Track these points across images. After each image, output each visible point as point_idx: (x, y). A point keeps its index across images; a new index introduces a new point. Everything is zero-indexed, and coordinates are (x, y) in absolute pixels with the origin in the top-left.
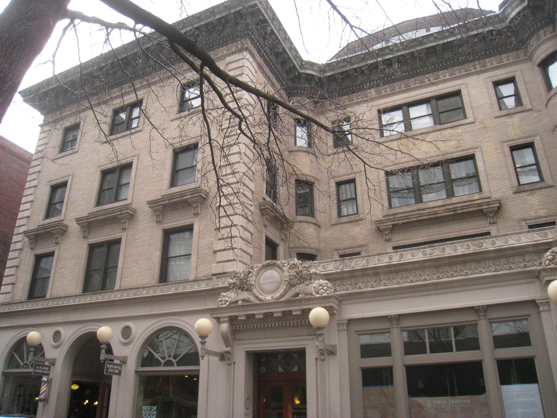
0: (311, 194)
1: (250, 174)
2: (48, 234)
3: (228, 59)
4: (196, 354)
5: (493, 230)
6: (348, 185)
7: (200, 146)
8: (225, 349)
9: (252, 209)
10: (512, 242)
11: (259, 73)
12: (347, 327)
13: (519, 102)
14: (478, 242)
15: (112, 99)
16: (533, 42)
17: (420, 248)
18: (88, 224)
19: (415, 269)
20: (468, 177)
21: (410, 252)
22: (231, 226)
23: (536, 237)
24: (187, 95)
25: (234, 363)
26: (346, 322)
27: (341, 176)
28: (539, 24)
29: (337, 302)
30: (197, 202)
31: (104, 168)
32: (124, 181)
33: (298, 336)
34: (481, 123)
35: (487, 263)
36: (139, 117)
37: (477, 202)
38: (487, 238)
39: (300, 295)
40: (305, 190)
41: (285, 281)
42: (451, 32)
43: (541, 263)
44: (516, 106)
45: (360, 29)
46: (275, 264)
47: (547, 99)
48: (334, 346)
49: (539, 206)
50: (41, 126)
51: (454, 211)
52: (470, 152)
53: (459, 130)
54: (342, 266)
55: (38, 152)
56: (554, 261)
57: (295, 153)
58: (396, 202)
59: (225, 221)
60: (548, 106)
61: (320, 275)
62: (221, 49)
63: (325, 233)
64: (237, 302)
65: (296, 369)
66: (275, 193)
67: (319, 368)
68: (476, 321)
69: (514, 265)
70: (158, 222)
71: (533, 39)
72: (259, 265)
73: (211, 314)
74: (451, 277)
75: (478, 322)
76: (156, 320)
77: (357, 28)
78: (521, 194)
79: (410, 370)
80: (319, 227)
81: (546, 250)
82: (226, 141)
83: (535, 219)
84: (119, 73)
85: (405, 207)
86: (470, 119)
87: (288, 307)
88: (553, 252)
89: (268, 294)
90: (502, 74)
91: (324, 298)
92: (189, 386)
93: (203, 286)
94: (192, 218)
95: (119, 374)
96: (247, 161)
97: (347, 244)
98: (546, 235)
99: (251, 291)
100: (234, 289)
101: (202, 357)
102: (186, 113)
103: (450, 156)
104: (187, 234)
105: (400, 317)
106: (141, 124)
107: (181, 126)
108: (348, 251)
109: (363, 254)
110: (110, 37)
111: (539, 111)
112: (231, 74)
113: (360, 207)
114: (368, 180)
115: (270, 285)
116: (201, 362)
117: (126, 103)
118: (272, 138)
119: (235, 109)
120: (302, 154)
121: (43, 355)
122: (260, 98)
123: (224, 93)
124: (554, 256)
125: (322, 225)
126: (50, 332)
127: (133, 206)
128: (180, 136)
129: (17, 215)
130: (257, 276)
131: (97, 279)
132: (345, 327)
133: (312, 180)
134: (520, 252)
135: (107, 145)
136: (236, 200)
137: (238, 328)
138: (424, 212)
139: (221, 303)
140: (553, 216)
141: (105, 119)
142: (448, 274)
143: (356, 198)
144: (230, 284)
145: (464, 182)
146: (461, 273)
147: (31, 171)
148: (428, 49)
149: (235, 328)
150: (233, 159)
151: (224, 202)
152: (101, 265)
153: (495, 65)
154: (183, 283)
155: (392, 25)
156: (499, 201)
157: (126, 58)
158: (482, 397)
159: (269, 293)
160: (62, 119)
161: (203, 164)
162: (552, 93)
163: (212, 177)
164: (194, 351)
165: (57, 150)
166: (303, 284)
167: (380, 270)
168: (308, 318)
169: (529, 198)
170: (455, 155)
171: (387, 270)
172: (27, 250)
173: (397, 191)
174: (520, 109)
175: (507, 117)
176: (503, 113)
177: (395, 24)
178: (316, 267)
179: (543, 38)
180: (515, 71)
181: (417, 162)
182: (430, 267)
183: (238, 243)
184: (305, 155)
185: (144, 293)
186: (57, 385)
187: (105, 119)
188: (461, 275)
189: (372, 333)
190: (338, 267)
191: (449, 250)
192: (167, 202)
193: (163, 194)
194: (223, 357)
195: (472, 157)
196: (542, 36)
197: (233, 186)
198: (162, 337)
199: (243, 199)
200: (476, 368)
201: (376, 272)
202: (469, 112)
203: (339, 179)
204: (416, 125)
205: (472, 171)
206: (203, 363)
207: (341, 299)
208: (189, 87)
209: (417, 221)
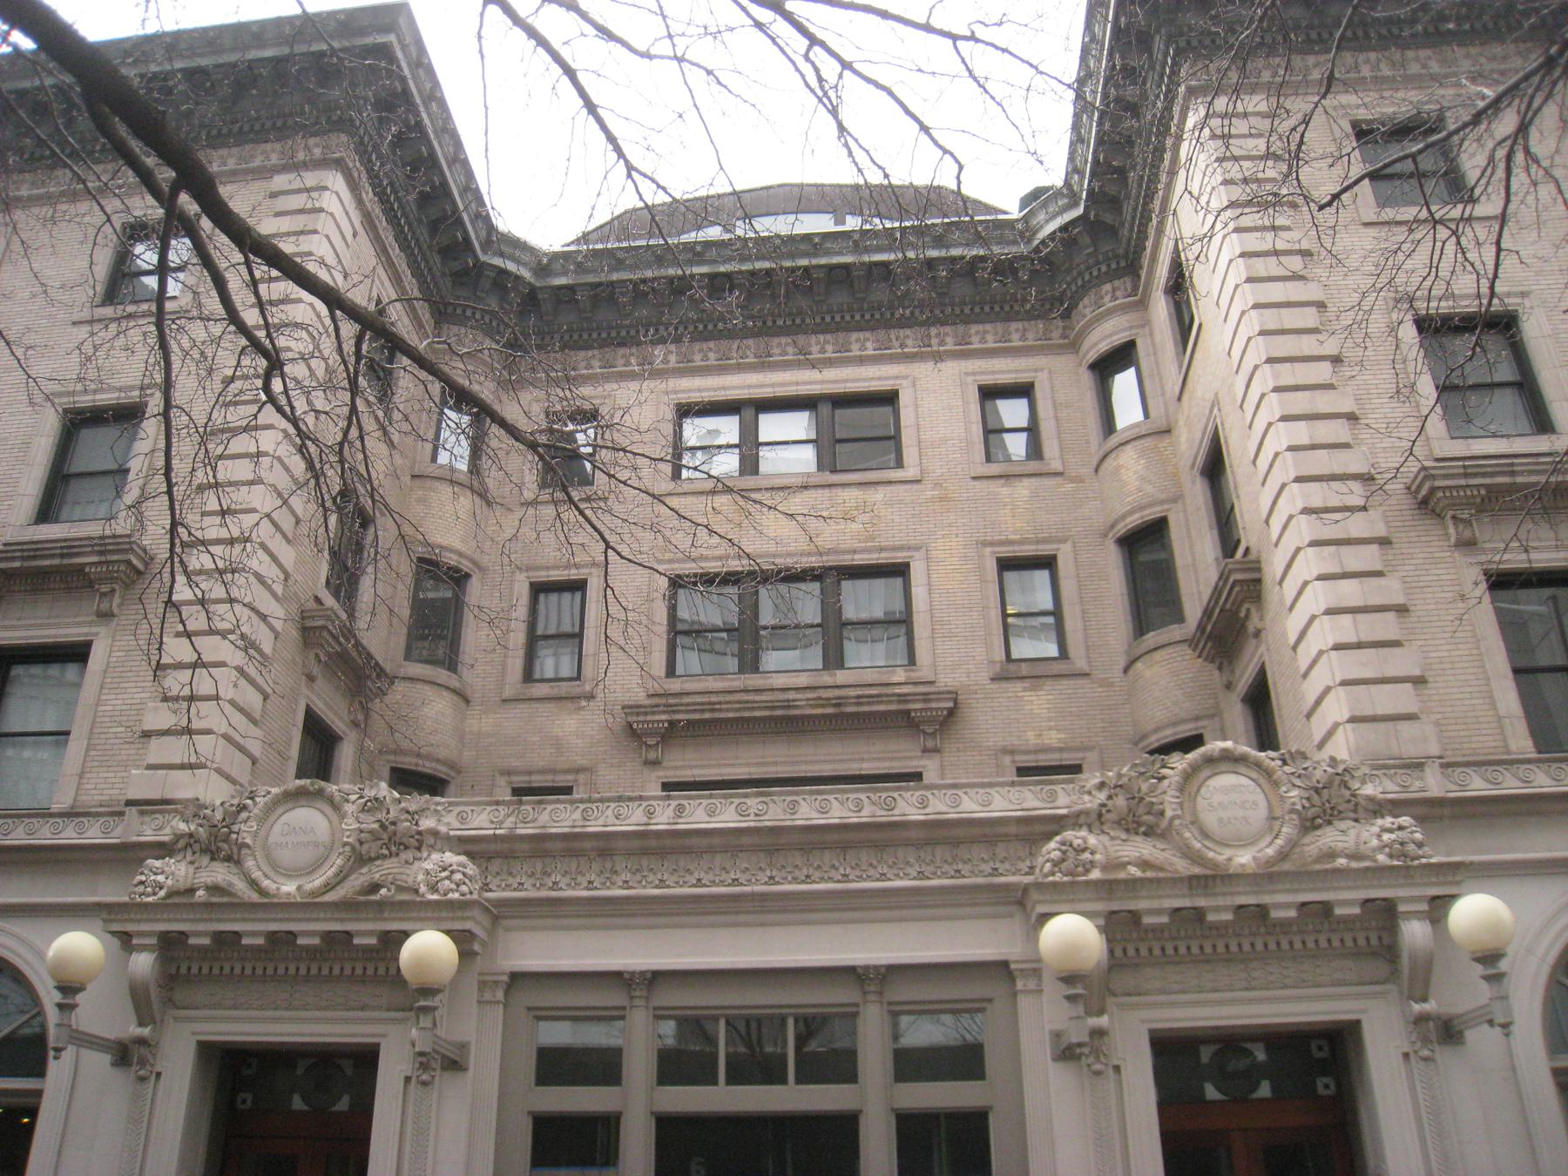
1: (287, 523)
4: (40, 1040)
5: (930, 768)
6: (567, 596)
8: (135, 1030)
10: (970, 806)
11: (363, 239)
12: (507, 992)
13: (1035, 449)
14: (884, 795)
16: (1086, 309)
17: (731, 796)
19: (712, 851)
20: (888, 622)
21: (705, 802)
22: (194, 666)
23: (1029, 800)
25: (159, 1075)
26: (505, 978)
27: (547, 568)
28: (1114, 266)
29: (485, 920)
30: (113, 580)
33: (362, 1009)
34: (937, 485)
35: (901, 853)
37: (897, 690)
38: (908, 789)
39: (383, 891)
41: (346, 844)
42: (857, 241)
43: (1032, 868)
44: (1029, 457)
45: (653, 181)
46: (320, 793)
47: (1102, 453)
48: (464, 1047)
49: (1050, 719)
51: (835, 705)
52: (899, 557)
53: (878, 495)
54: (512, 819)
56: (1064, 866)
57: (429, 483)
58: (689, 660)
60: (1101, 472)
61: (448, 838)
62: (263, 146)
63: (481, 722)
64: (191, 891)
65: (343, 1104)
67: (410, 1109)
68: (857, 1005)
69: (968, 867)
71: (1086, 301)
72: (275, 790)
73: (104, 920)
74: (803, 882)
75: (861, 1009)
77: (645, 175)
78: (1005, 685)
79: (669, 1128)
80: (467, 701)
81: (1049, 836)
83: (1036, 752)
85: (708, 678)
86: (910, 472)
87: (342, 920)
88: (1063, 843)
89: (289, 877)
90: (1004, 370)
93: (93, 834)
94: (90, 624)
97: (539, 759)
98: (1053, 796)
99: (238, 863)
100: (189, 853)
101: (58, 1050)
103: (846, 560)
104: (71, 670)
105: (656, 978)
107: (88, 348)
108: (538, 780)
111: (1079, 480)
113: (588, 663)
114: (609, 592)
115: (300, 850)
116: (53, 1067)
118: (354, 433)
119: (258, 327)
120: (446, 490)
122: (338, 312)
124: (1064, 852)
128: (80, 379)
130: (262, 820)
132: (500, 995)
133: (466, 566)
134: (985, 833)
137: (183, 971)
138: (757, 698)
139: (141, 888)
140: (1078, 749)
142: (797, 873)
143: (579, 636)
144: (178, 837)
145: (878, 632)
146: (833, 873)
148: (831, 268)
149: (173, 970)
150: (226, 471)
153: (991, 345)
154: (30, 816)
155: (730, 190)
156: (954, 696)
159: (290, 874)
162: (1114, 440)
163: (157, 517)
164: (37, 1030)
166: (394, 860)
168: (397, 959)
169: (1029, 696)
170: (860, 559)
171: (637, 843)
173: (698, 632)
174: (1034, 466)
175: (1002, 481)
176: (994, 469)
177: (738, 188)
178: (439, 816)
179: (1109, 304)
180: (1036, 370)
181: (745, 562)
182: (754, 849)
184: (452, 497)
188: (830, 879)
189: (580, 1017)
190: (502, 822)
191: (808, 810)
192: (17, 564)
193: (9, 539)
194: (123, 1054)
195: (900, 571)
196: (1107, 298)
197: (214, 549)
201: (605, 847)
202: (910, 453)
203: (542, 576)
204: (771, 462)
205: (898, 606)
206: (58, 1071)
207: (500, 913)
209: (737, 719)
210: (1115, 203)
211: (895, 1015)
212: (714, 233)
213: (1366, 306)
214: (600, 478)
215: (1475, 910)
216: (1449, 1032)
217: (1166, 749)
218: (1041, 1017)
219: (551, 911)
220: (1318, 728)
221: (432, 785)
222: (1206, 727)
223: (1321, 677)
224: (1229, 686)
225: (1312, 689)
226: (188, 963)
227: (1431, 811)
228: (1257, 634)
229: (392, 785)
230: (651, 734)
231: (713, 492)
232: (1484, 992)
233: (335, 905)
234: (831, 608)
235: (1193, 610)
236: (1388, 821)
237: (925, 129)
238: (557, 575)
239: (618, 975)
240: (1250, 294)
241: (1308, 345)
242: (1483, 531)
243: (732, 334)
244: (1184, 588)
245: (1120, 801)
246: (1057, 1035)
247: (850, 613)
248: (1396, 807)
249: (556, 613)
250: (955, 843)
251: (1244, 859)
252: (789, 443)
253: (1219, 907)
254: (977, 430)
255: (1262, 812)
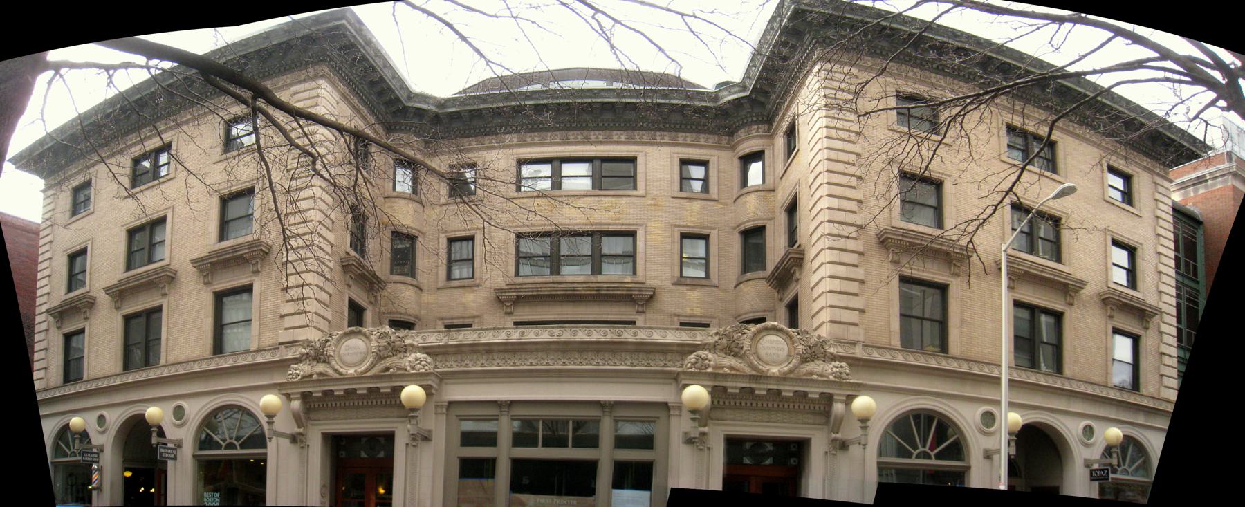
0: (413, 249)
1: (328, 223)
2: (73, 310)
3: (293, 89)
4: (262, 436)
5: (640, 320)
6: (464, 243)
7: (256, 191)
9: (331, 265)
10: (657, 337)
13: (706, 188)
15: (129, 147)
16: (742, 133)
18: (119, 293)
19: (537, 351)
20: (624, 256)
23: (684, 337)
24: (234, 132)
29: (437, 381)
31: (130, 226)
32: (158, 239)
36: (168, 163)
40: (404, 250)
46: (360, 332)
48: (430, 431)
50: (44, 191)
52: (632, 228)
53: (624, 201)
55: (45, 220)
59: (293, 280)
63: (427, 298)
64: (311, 375)
66: (363, 246)
70: (207, 284)
76: (212, 398)
79: (517, 464)
81: (691, 352)
82: (294, 183)
84: (134, 117)
85: (533, 277)
86: (640, 192)
91: (421, 374)
92: (256, 471)
93: (268, 357)
95: (175, 458)
96: (324, 207)
97: (455, 313)
98: (695, 336)
102: (236, 153)
103: (605, 228)
104: (245, 296)
105: (512, 403)
106: (172, 170)
108: (456, 322)
109: (475, 327)
110: (114, 79)
111: (726, 204)
112: (299, 105)
115: (354, 355)
116: (269, 444)
117: (148, 149)
120: (402, 202)
121: (90, 442)
123: (288, 128)
125: (425, 288)
126: (92, 417)
127: (173, 267)
129: (35, 293)
130: (336, 345)
131: (138, 354)
133: (415, 233)
135: (130, 200)
136: (309, 254)
141: (123, 171)
143: (473, 260)
145: (618, 260)
147: (41, 242)
151: (292, 257)
152: (142, 338)
156: (654, 290)
157: (140, 99)
158: (591, 499)
159: (351, 366)
160: (68, 179)
161: (263, 213)
162: (746, 190)
165: (68, 214)
167: (495, 348)
169: (689, 293)
170: (612, 228)
171: (502, 348)
172: (53, 329)
173: (530, 257)
174: (704, 196)
176: (684, 194)
178: (412, 338)
179: (754, 133)
182: (556, 350)
183: (312, 306)
185: (196, 368)
186: (109, 473)
187: (123, 171)
191: (582, 335)
194: (294, 439)
195: (632, 234)
197: (305, 237)
198: (221, 416)
199: (319, 253)
200: (590, 468)
201: (489, 349)
203: (452, 235)
204: (567, 184)
205: (630, 249)
206: (271, 447)
207: (443, 377)
208: (237, 123)
210: (766, 94)
211: (616, 421)
212: (538, 87)
213: (872, 159)
214: (479, 192)
215: (863, 402)
216: (844, 446)
217: (748, 322)
218: (680, 426)
219: (466, 376)
220: (816, 323)
221: (408, 325)
222: (768, 315)
223: (821, 302)
224: (781, 300)
225: (816, 306)
226: (314, 403)
227: (855, 363)
228: (797, 280)
229: (391, 326)
230: (508, 301)
231: (538, 197)
232: (859, 432)
233: (371, 377)
234: (596, 249)
235: (771, 264)
236: (837, 363)
237: (660, 49)
238: (459, 234)
239: (495, 402)
240: (825, 143)
241: (852, 170)
242: (904, 260)
243: (548, 130)
244: (768, 257)
245: (724, 341)
246: (686, 433)
247: (605, 251)
248: (841, 358)
249: (461, 250)
250: (648, 352)
251: (775, 370)
252: (577, 177)
253: (761, 389)
254: (677, 177)
255: (785, 353)
